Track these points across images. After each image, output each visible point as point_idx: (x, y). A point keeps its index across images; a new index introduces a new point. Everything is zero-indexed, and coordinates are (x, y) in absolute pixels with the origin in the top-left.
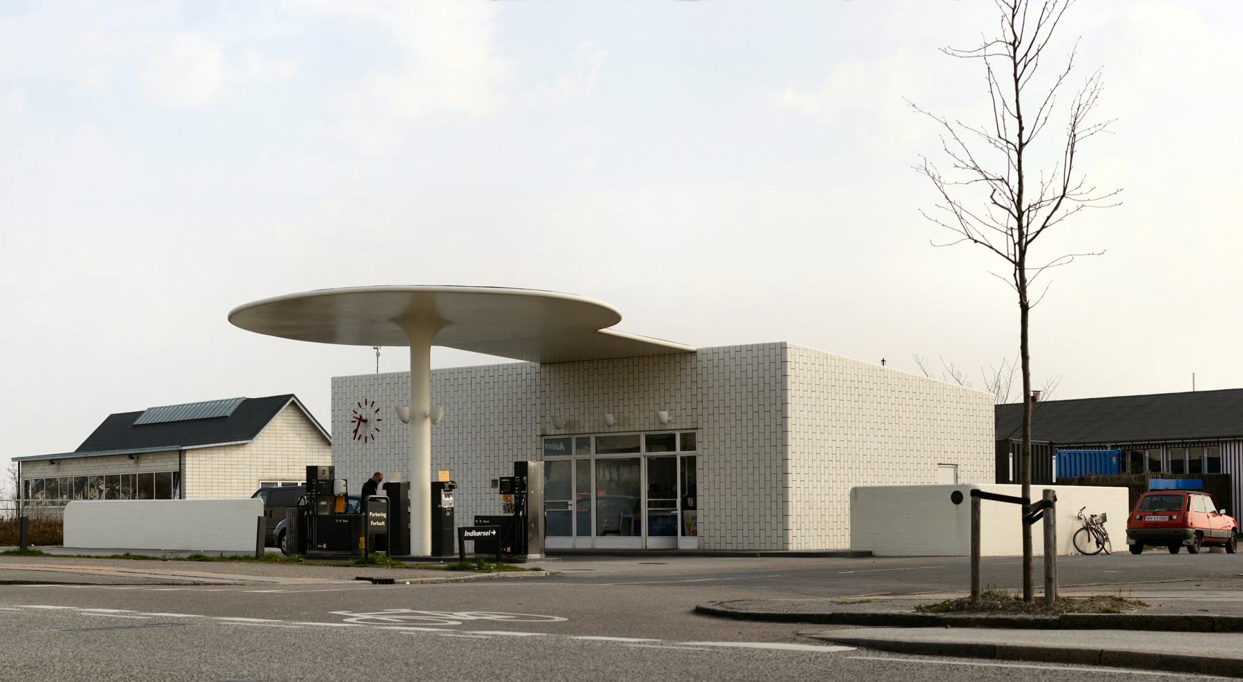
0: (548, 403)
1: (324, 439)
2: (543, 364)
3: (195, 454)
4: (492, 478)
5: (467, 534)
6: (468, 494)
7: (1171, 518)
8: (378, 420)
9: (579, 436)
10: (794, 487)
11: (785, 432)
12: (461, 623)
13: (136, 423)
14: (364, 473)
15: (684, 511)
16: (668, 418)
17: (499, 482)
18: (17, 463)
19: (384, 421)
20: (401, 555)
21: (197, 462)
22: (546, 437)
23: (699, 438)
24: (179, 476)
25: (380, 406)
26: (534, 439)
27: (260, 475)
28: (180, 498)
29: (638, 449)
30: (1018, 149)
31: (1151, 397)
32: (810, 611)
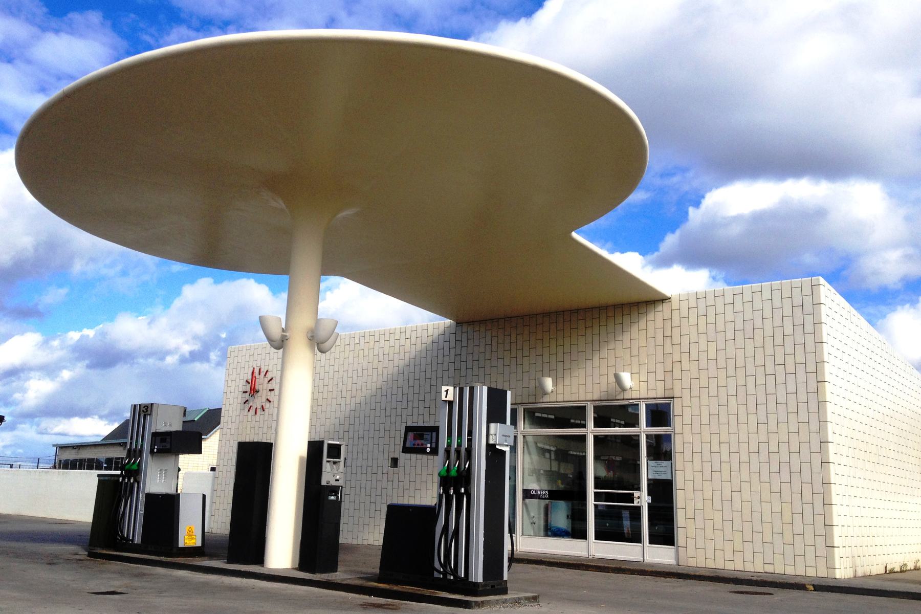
0: (463, 368)
1: (663, 175)
2: (459, 323)
4: (392, 455)
7: (615, 458)
8: (270, 390)
10: (232, 442)
11: (821, 403)
12: (125, 536)
13: (282, 349)
14: (384, 497)
15: (492, 425)
26: (688, 448)
29: (634, 422)
31: (609, 561)
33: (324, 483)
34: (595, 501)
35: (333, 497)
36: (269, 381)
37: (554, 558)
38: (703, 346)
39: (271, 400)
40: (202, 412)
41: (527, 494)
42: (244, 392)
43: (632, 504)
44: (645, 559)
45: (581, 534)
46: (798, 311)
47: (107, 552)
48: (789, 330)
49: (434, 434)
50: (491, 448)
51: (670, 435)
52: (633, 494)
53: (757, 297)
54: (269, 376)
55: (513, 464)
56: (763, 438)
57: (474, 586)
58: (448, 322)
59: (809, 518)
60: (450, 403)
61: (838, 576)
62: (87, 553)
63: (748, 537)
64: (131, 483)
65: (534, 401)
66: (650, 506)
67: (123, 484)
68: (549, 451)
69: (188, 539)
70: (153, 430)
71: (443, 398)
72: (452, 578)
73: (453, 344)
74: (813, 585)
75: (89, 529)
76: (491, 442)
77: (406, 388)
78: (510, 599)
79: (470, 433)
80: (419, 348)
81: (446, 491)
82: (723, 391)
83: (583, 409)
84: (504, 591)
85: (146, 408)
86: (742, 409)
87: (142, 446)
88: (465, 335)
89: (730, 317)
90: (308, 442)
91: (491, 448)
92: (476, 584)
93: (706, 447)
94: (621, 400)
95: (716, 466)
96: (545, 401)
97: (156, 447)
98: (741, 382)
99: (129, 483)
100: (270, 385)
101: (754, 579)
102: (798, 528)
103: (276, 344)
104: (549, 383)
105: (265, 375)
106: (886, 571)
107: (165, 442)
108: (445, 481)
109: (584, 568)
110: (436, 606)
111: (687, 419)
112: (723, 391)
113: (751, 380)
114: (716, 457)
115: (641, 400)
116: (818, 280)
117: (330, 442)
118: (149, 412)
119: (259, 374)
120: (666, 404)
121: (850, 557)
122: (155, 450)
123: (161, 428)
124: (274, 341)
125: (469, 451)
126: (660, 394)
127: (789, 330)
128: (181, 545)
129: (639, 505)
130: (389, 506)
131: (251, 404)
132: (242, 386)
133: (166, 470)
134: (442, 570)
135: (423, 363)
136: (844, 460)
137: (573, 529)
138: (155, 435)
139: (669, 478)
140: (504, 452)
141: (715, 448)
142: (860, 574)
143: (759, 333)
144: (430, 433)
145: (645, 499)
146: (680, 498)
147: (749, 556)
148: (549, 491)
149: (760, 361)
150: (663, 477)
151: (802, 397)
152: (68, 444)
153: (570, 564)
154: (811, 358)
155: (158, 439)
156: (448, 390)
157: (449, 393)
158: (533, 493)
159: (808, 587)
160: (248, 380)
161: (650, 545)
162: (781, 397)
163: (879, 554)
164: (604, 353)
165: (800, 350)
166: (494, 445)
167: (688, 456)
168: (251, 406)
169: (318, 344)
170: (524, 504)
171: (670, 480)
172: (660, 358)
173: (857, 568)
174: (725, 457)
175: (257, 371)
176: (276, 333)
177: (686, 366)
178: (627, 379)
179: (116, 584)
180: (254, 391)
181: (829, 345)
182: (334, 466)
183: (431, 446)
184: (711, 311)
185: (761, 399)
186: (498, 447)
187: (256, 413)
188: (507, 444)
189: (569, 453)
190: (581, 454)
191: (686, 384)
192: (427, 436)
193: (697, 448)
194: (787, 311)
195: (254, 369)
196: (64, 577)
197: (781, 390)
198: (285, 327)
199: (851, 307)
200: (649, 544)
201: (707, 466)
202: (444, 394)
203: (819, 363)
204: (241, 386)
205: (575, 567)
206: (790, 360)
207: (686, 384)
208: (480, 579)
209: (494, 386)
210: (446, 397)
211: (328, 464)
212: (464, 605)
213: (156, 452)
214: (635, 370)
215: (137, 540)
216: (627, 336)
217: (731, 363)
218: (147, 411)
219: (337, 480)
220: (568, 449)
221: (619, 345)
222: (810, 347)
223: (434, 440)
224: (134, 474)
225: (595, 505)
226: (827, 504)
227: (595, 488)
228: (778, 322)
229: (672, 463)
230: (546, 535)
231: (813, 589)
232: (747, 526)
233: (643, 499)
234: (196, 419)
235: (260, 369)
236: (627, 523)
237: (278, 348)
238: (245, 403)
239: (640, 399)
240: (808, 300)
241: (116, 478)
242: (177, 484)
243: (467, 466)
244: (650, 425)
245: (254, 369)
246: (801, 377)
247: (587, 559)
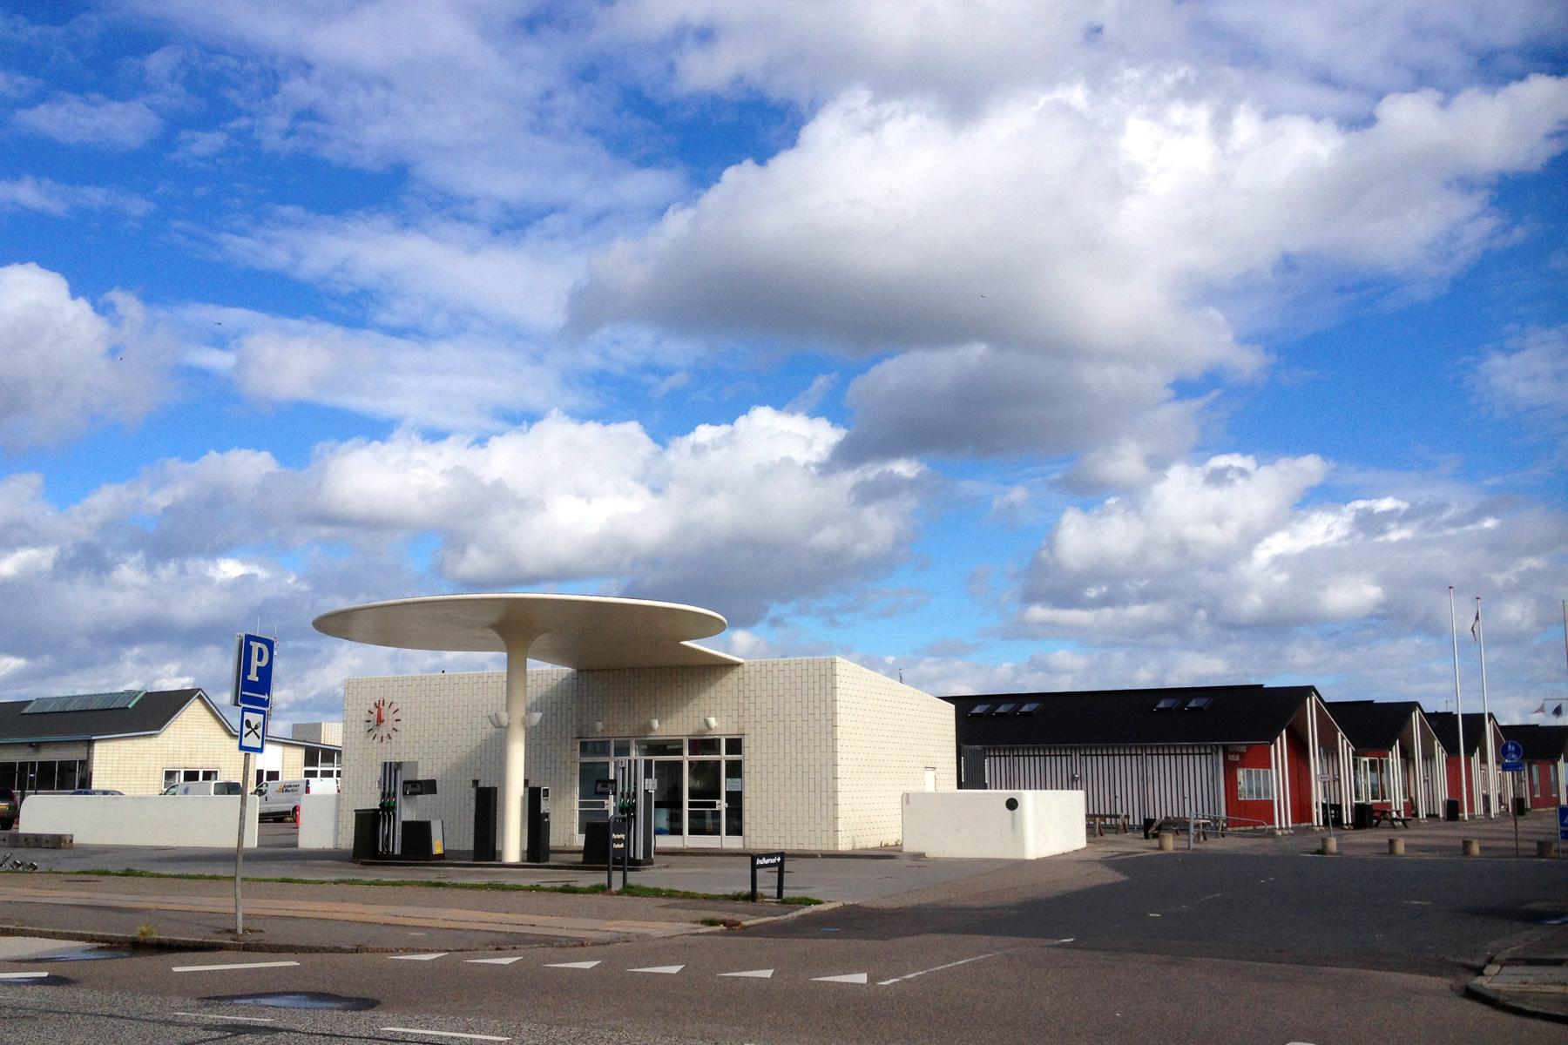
2: (579, 671)
3: (104, 744)
5: (759, 862)
6: (476, 729)
8: (397, 720)
9: (618, 739)
11: (835, 739)
16: (719, 725)
19: (403, 722)
20: (539, 862)
21: (105, 751)
22: (581, 740)
23: (745, 743)
24: (86, 764)
25: (399, 707)
27: (164, 764)
28: (385, 763)
32: (177, 958)
33: (542, 812)
40: (136, 696)
45: (677, 831)
50: (646, 791)
54: (394, 707)
58: (570, 670)
61: (840, 849)
66: (726, 809)
79: (635, 784)
83: (680, 742)
84: (652, 864)
91: (646, 791)
93: (793, 724)
104: (656, 723)
125: (635, 795)
135: (549, 701)
138: (406, 783)
147: (789, 840)
167: (753, 774)
178: (713, 721)
192: (610, 785)
201: (764, 782)
215: (397, 851)
222: (829, 703)
233: (722, 805)
234: (130, 706)
236: (709, 821)
246: (824, 723)
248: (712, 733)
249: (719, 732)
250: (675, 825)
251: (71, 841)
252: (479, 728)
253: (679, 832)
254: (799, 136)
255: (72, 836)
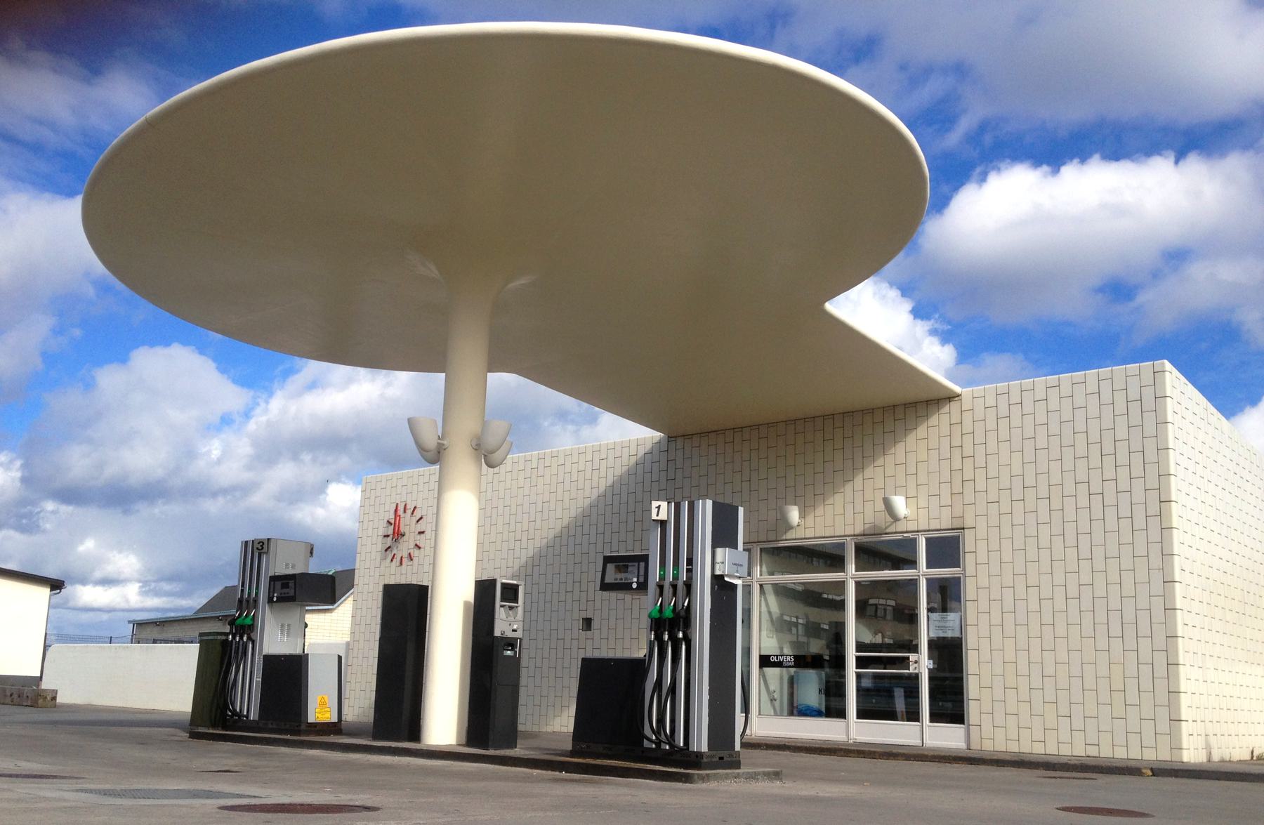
2: (671, 438)
8: (420, 533)
12: (238, 710)
15: (719, 551)
17: (284, 581)
18: (132, 625)
20: (486, 747)
23: (968, 542)
26: (983, 595)
29: (912, 563)
30: (667, 741)
33: (497, 633)
34: (856, 668)
35: (509, 652)
36: (418, 521)
37: (803, 743)
38: (1004, 459)
39: (420, 546)
41: (765, 661)
42: (385, 536)
43: (908, 671)
44: (925, 742)
45: (835, 710)
46: (1135, 408)
47: (215, 732)
48: (1122, 433)
49: (642, 564)
50: (718, 580)
51: (959, 578)
52: (908, 658)
53: (1079, 390)
54: (418, 514)
55: (746, 607)
56: (1085, 578)
57: (697, 756)
58: (662, 435)
59: (1146, 684)
60: (663, 523)
61: (1185, 759)
62: (188, 735)
63: (1064, 710)
64: (244, 642)
65: (774, 538)
67: (234, 643)
68: (796, 625)
69: (320, 713)
70: (271, 573)
71: (654, 517)
72: (667, 747)
73: (663, 466)
74: (1152, 769)
75: (189, 718)
76: (718, 572)
77: (601, 525)
78: (743, 773)
80: (618, 472)
81: (659, 638)
82: (1031, 518)
83: (842, 546)
84: (736, 764)
85: (261, 544)
86: (1058, 542)
87: (257, 594)
88: (680, 453)
89: (1041, 418)
90: (476, 581)
91: (718, 580)
92: (699, 755)
94: (892, 533)
95: (1021, 618)
96: (788, 538)
97: (275, 595)
98: (1056, 504)
99: (241, 643)
100: (419, 525)
101: (1072, 762)
102: (1132, 697)
103: (430, 455)
104: (794, 514)
105: (412, 514)
106: (1252, 757)
107: (288, 588)
108: (658, 625)
109: (843, 753)
110: (648, 781)
111: (982, 557)
112: (1031, 518)
113: (1070, 502)
114: (1021, 605)
115: (920, 533)
116: (1163, 365)
117: (504, 581)
118: (265, 550)
119: (405, 512)
120: (952, 537)
121: (1203, 735)
122: (275, 599)
123: (281, 570)
124: (427, 452)
125: (689, 586)
126: (946, 524)
127: (1122, 433)
128: (311, 719)
129: (916, 671)
130: (583, 660)
131: (395, 551)
132: (382, 528)
133: (289, 625)
134: (654, 738)
136: (1196, 607)
137: (828, 708)
138: (274, 579)
139: (957, 634)
140: (734, 587)
141: (1021, 592)
142: (1216, 758)
143: (1081, 439)
144: (636, 564)
145: (924, 664)
146: (973, 662)
148: (795, 657)
149: (1082, 476)
150: (949, 634)
151: (1140, 522)
152: (148, 620)
153: (823, 748)
154: (1152, 471)
155: (278, 584)
156: (660, 506)
157: (661, 510)
158: (774, 659)
159: (1144, 771)
160: (390, 521)
161: (931, 724)
162: (1111, 524)
163: (1241, 684)
164: (869, 472)
165: (1137, 459)
166: (722, 577)
167: (983, 605)
168: (394, 555)
169: (485, 456)
170: (763, 676)
171: (958, 638)
172: (946, 476)
173: (1212, 750)
174: (1034, 606)
175: (401, 512)
176: (430, 441)
177: (981, 486)
178: (899, 503)
179: (230, 763)
180: (398, 535)
181: (1181, 531)
182: (511, 612)
183: (638, 580)
184: (1016, 410)
185: (1084, 526)
186: (726, 579)
187: (401, 564)
188: (738, 575)
189: (822, 626)
190: (838, 598)
191: (981, 509)
192: (633, 568)
193: (995, 594)
194: (1121, 406)
195: (397, 504)
196: (164, 756)
197: (1111, 514)
198: (442, 435)
199: (1208, 403)
200: (931, 722)
202: (654, 511)
203: (1164, 475)
204: (381, 527)
205: (830, 752)
206: (1123, 474)
207: (981, 509)
208: (704, 748)
209: (720, 499)
210: (657, 515)
211: (502, 609)
212: (683, 779)
213: (276, 602)
214: (912, 492)
215: (253, 716)
216: (900, 447)
217: (1043, 479)
218: (263, 548)
219: (514, 631)
220: (820, 591)
221: (889, 459)
222: (1151, 455)
223: (642, 572)
224: (246, 630)
225: (856, 672)
226: (1172, 664)
227: (857, 651)
228: (1107, 423)
229: (961, 616)
230: (791, 714)
231: (1151, 774)
232: (1063, 695)
233: (922, 664)
235: (405, 505)
237: (433, 462)
238: (386, 550)
239: (918, 531)
240: (1148, 393)
241: (224, 638)
242: (304, 644)
243: (686, 604)
244: (932, 675)
245: (397, 504)
246: (1139, 496)
247: (847, 743)
248: (901, 526)
249: (912, 527)
250: (834, 703)
251: (54, 698)
252: (524, 539)
253: (841, 713)
254: (983, 179)
255: (55, 692)
